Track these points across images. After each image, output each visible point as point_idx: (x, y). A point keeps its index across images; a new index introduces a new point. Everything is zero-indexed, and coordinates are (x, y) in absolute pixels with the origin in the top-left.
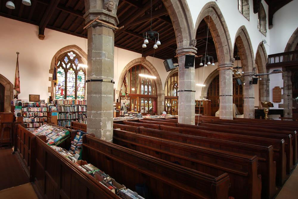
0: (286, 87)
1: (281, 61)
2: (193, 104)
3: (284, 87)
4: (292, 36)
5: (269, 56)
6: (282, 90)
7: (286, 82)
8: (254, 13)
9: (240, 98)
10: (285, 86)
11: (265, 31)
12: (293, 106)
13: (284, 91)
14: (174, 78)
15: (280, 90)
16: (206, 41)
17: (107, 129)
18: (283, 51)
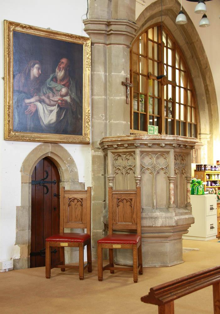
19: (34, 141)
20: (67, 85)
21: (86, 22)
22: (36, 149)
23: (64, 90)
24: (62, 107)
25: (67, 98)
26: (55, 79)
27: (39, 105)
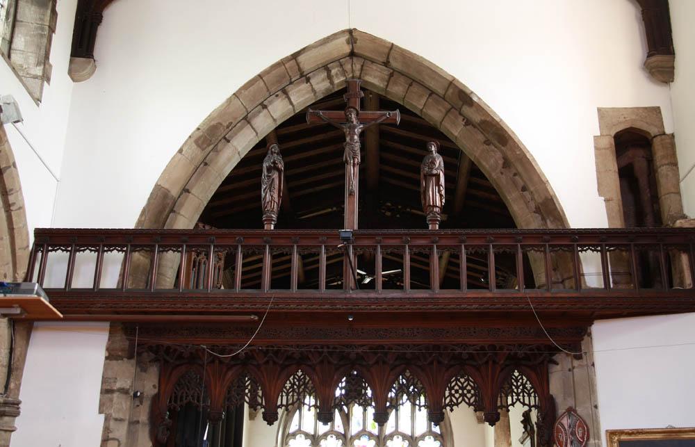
1: (110, 281)
4: (180, 151)
5: (40, 233)
9: (317, 287)
11: (38, 71)
18: (127, 219)
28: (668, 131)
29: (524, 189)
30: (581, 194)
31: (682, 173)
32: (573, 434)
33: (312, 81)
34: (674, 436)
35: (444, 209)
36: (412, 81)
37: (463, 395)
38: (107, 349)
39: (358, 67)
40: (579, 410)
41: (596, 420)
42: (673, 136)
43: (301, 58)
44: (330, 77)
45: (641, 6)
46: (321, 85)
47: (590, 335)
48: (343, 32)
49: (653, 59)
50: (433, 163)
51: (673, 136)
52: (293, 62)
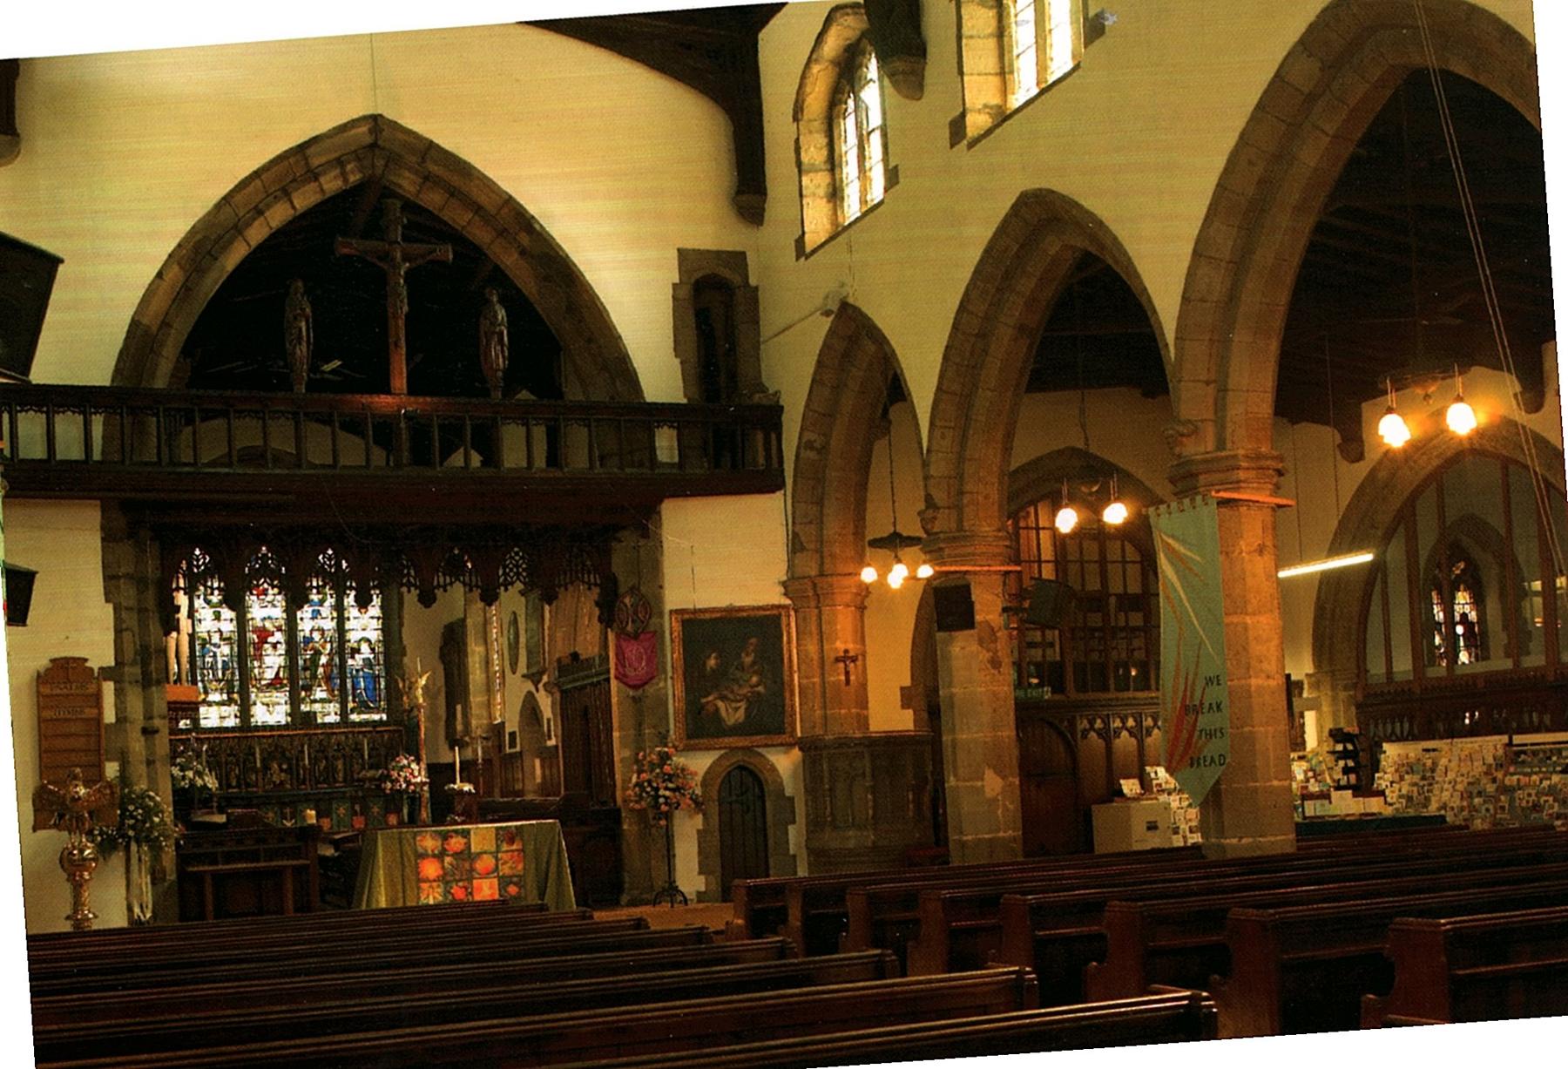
0: (133, 663)
2: (1533, 416)
3: (119, 662)
6: (109, 688)
7: (131, 620)
8: (1068, 185)
10: (129, 654)
12: (101, 669)
13: (119, 693)
14: (264, 427)
15: (92, 689)
16: (804, 681)
17: (270, 422)
19: (708, 749)
20: (760, 673)
21: (784, 584)
22: (721, 757)
23: (755, 679)
24: (754, 701)
25: (760, 689)
26: (741, 667)
27: (720, 704)
28: (753, 281)
29: (590, 341)
30: (655, 360)
31: (766, 330)
32: (636, 613)
33: (322, 180)
34: (734, 614)
35: (505, 371)
36: (453, 192)
37: (518, 574)
38: (103, 528)
39: (380, 163)
40: (643, 589)
41: (659, 599)
42: (757, 288)
43: (309, 152)
44: (344, 175)
45: (731, 118)
46: (332, 184)
47: (659, 513)
48: (365, 118)
49: (744, 198)
50: (495, 317)
51: (757, 288)
52: (299, 157)
